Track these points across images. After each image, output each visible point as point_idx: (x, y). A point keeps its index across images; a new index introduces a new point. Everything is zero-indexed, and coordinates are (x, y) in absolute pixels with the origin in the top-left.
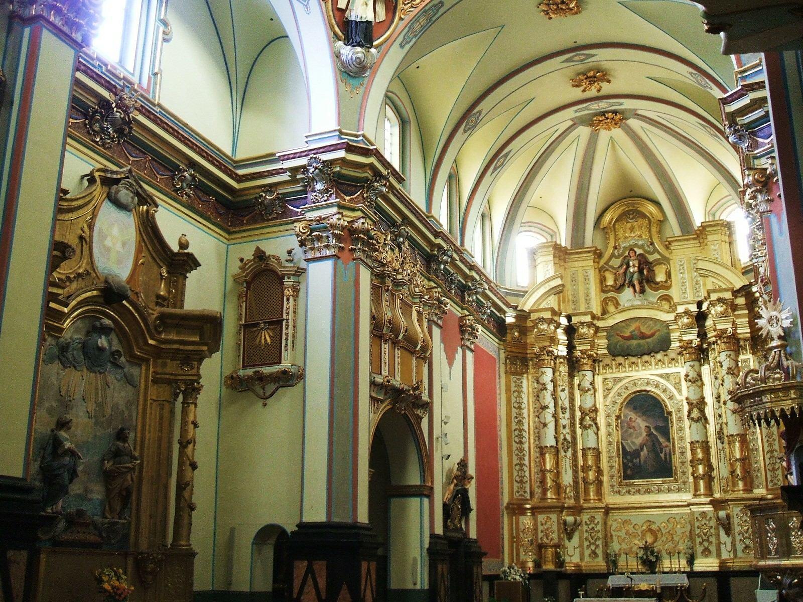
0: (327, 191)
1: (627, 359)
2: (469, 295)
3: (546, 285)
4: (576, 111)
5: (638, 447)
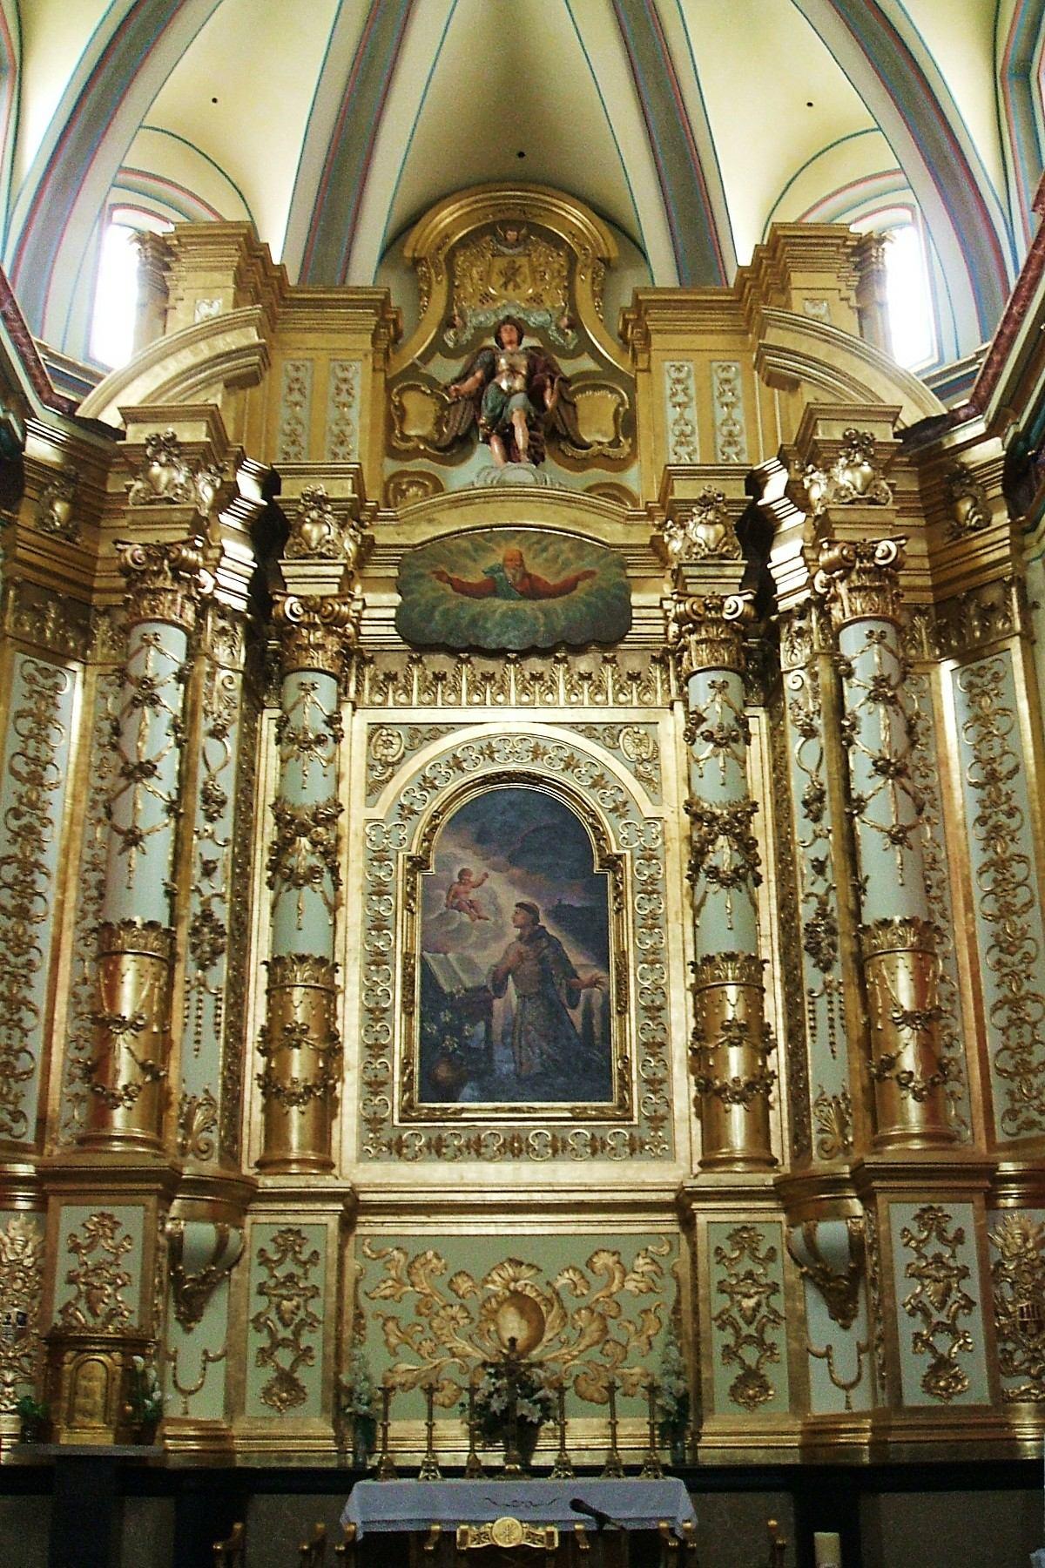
5: (483, 980)
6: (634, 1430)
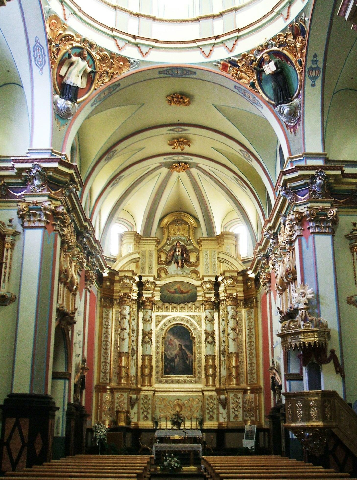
0: (42, 186)
1: (171, 304)
2: (91, 258)
3: (130, 257)
4: (165, 159)
5: (174, 356)
6: (195, 424)
